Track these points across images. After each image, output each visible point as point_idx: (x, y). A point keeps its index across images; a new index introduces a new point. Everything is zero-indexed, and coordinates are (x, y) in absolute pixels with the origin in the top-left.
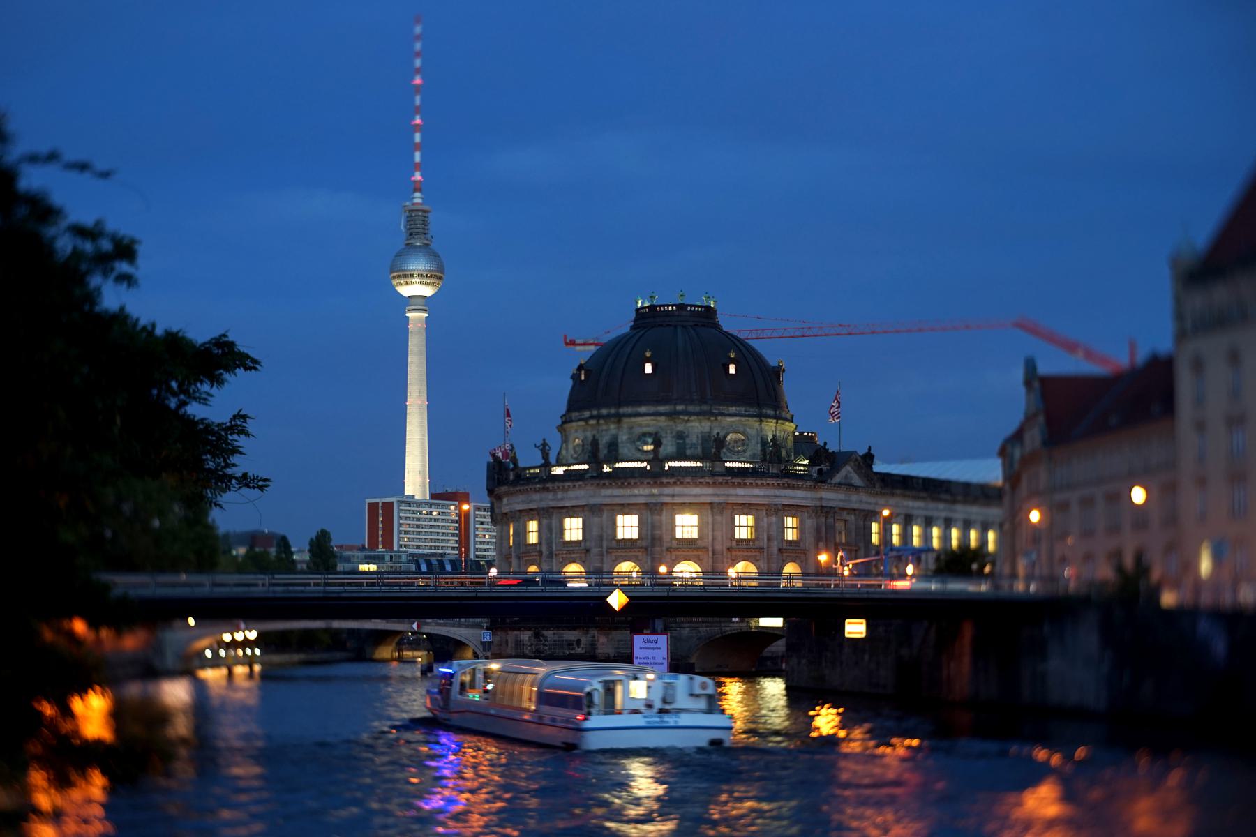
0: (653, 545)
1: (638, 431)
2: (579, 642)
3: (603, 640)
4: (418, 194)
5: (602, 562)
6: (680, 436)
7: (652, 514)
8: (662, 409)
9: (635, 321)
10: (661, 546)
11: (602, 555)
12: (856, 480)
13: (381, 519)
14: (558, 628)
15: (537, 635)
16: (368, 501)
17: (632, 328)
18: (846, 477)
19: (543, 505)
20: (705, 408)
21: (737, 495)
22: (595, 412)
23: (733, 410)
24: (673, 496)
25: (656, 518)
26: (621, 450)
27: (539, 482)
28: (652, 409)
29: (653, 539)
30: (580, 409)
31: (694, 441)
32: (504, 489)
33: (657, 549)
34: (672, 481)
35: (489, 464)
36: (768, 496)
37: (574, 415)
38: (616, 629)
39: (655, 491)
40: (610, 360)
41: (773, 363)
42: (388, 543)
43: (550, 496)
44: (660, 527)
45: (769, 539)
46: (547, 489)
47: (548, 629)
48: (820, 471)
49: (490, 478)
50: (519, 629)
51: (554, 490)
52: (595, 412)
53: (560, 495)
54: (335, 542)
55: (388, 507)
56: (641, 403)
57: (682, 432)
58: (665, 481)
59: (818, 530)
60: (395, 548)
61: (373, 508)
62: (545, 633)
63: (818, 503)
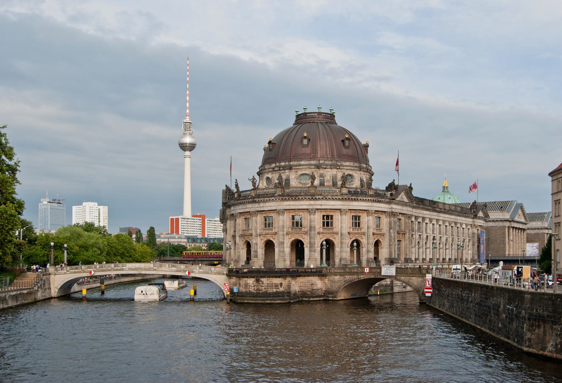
0: (310, 230)
1: (300, 172)
2: (281, 284)
3: (293, 282)
4: (188, 117)
5: (284, 239)
6: (322, 176)
7: (310, 215)
8: (312, 162)
9: (296, 121)
10: (315, 231)
11: (284, 235)
12: (406, 200)
13: (175, 225)
14: (269, 277)
15: (258, 281)
16: (171, 217)
17: (294, 124)
18: (402, 198)
19: (253, 210)
20: (334, 162)
21: (353, 206)
22: (278, 164)
23: (347, 164)
24: (321, 205)
25: (312, 216)
26: (291, 183)
27: (251, 198)
28: (307, 163)
29: (311, 227)
30: (270, 163)
31: (329, 178)
32: (233, 202)
33: (313, 232)
34: (321, 197)
35: (223, 191)
36: (368, 206)
37: (267, 166)
38: (300, 276)
39: (312, 202)
40: (285, 138)
41: (363, 142)
42: (177, 232)
43: (257, 205)
44: (314, 221)
45: (368, 228)
46: (255, 202)
47: (264, 277)
48: (391, 194)
49: (224, 197)
50: (247, 277)
51: (259, 202)
52: (278, 164)
53: (262, 205)
54: (157, 233)
55: (177, 220)
56: (301, 160)
57: (323, 174)
58: (317, 197)
59: (390, 224)
60: (180, 233)
61: (172, 220)
62: (263, 279)
63: (390, 210)
